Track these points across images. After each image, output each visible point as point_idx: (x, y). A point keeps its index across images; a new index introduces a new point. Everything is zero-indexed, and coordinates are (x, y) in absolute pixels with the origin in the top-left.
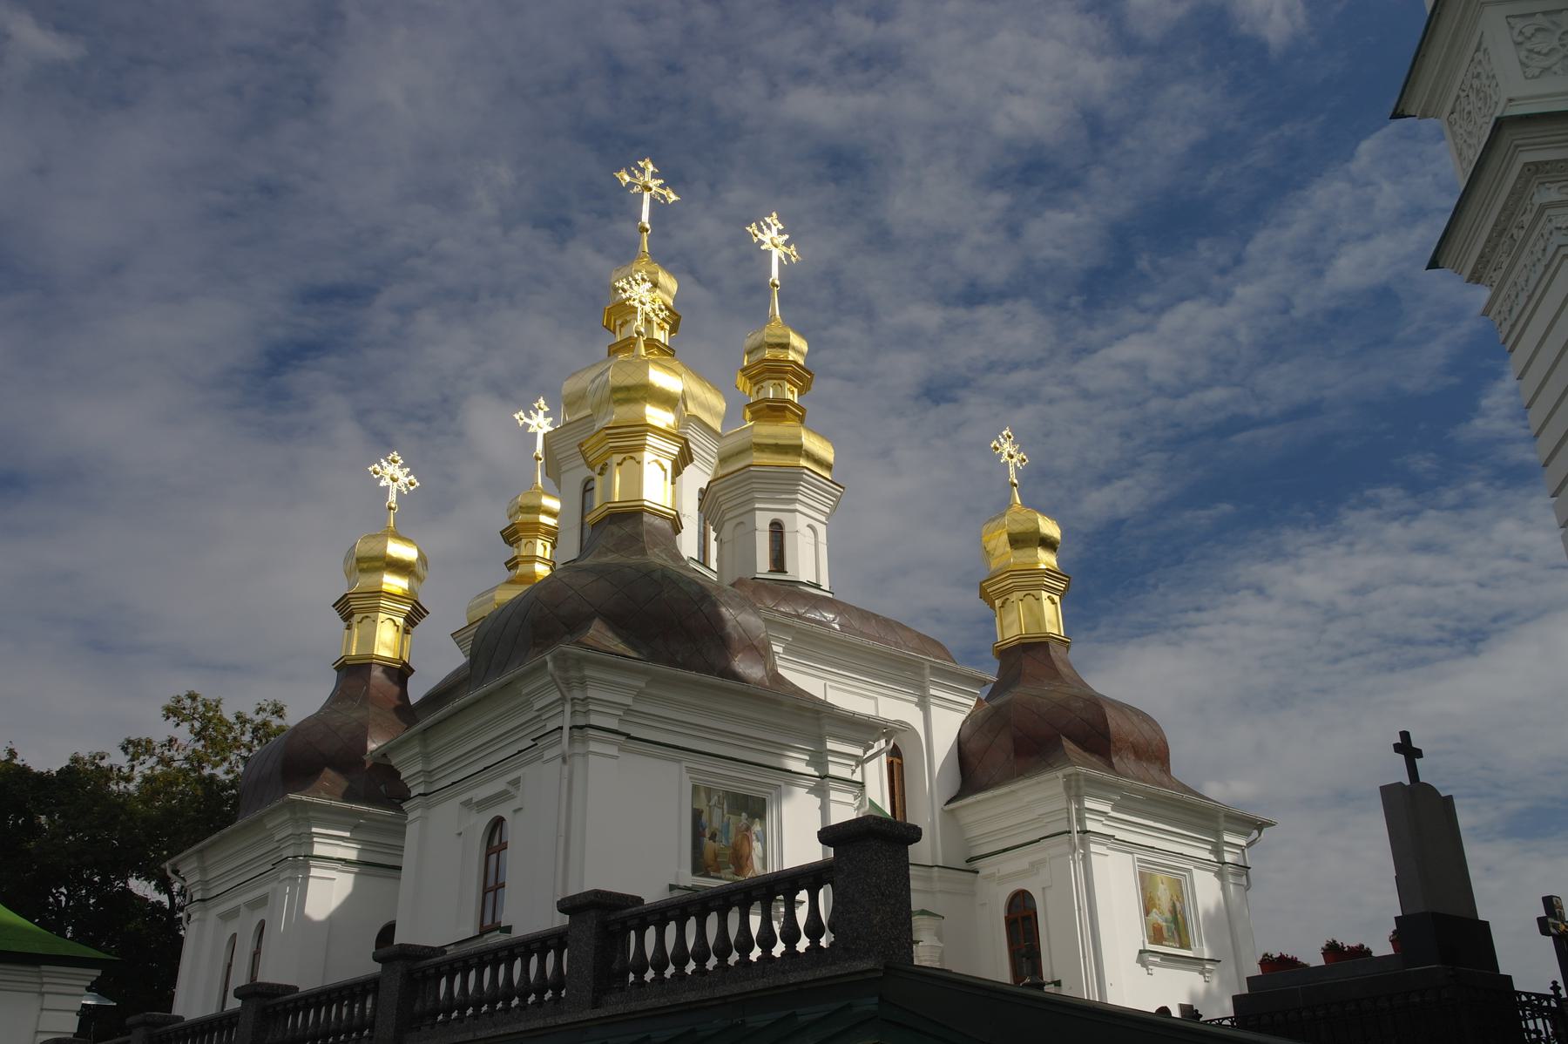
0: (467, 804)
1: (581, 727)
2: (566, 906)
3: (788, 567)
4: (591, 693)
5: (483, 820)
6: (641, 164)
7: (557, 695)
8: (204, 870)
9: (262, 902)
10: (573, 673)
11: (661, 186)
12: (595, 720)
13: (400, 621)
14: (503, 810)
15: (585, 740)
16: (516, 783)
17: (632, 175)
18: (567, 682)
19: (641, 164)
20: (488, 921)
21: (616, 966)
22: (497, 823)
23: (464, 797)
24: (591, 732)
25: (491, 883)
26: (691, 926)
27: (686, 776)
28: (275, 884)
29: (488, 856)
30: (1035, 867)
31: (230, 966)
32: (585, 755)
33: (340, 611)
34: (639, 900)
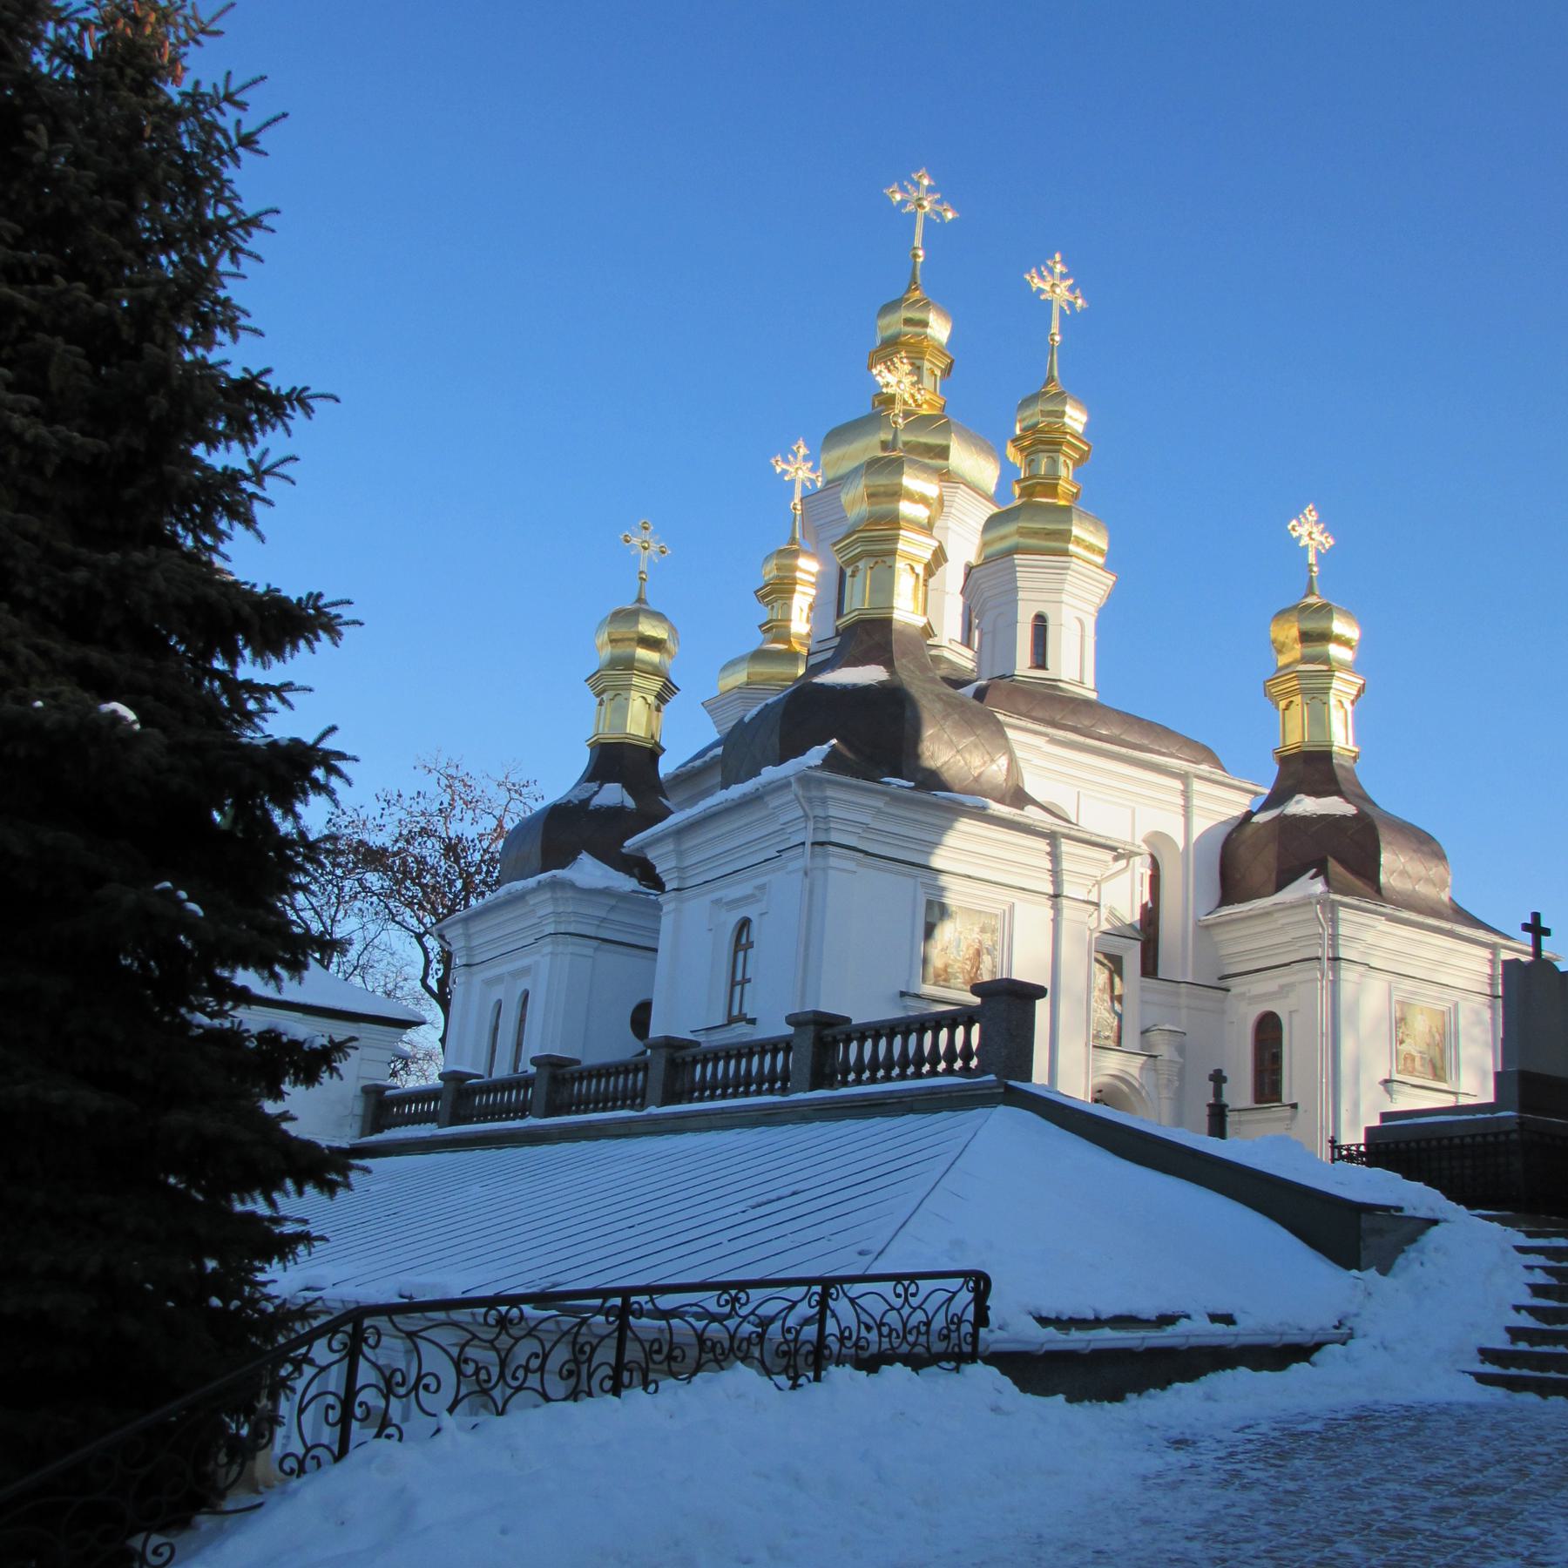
0: (717, 902)
1: (822, 844)
2: (792, 1020)
3: (1049, 664)
4: (832, 812)
5: (733, 918)
6: (915, 177)
7: (801, 813)
8: (468, 937)
9: (526, 971)
10: (814, 793)
11: (938, 202)
12: (835, 837)
13: (651, 699)
14: (750, 912)
15: (826, 856)
16: (762, 887)
17: (903, 190)
18: (810, 800)
19: (915, 177)
20: (735, 1012)
21: (827, 1070)
22: (745, 924)
23: (717, 895)
24: (831, 848)
25: (739, 977)
26: (944, 1034)
27: (921, 891)
28: (537, 957)
29: (736, 953)
30: (1284, 991)
31: (496, 1028)
32: (825, 869)
33: (593, 687)
34: (848, 1020)
